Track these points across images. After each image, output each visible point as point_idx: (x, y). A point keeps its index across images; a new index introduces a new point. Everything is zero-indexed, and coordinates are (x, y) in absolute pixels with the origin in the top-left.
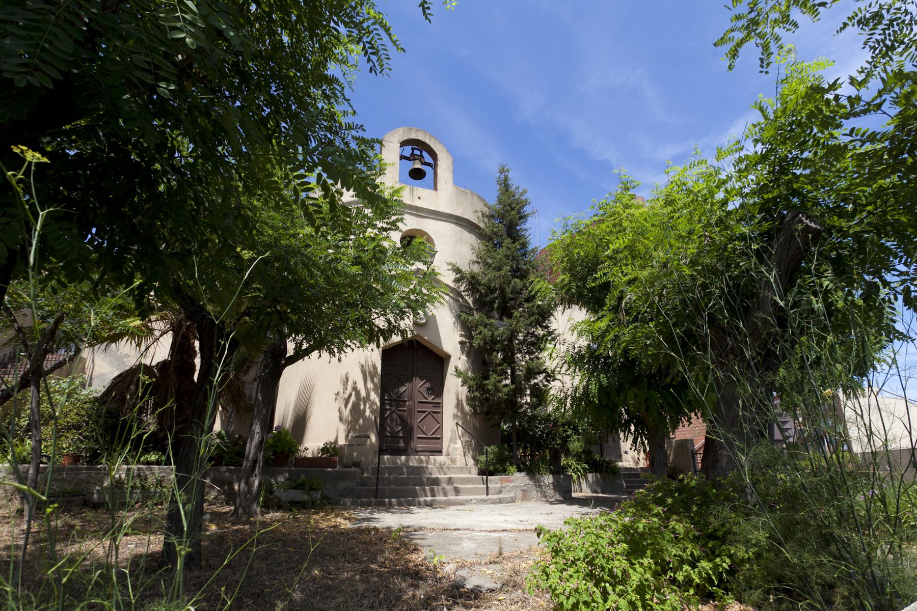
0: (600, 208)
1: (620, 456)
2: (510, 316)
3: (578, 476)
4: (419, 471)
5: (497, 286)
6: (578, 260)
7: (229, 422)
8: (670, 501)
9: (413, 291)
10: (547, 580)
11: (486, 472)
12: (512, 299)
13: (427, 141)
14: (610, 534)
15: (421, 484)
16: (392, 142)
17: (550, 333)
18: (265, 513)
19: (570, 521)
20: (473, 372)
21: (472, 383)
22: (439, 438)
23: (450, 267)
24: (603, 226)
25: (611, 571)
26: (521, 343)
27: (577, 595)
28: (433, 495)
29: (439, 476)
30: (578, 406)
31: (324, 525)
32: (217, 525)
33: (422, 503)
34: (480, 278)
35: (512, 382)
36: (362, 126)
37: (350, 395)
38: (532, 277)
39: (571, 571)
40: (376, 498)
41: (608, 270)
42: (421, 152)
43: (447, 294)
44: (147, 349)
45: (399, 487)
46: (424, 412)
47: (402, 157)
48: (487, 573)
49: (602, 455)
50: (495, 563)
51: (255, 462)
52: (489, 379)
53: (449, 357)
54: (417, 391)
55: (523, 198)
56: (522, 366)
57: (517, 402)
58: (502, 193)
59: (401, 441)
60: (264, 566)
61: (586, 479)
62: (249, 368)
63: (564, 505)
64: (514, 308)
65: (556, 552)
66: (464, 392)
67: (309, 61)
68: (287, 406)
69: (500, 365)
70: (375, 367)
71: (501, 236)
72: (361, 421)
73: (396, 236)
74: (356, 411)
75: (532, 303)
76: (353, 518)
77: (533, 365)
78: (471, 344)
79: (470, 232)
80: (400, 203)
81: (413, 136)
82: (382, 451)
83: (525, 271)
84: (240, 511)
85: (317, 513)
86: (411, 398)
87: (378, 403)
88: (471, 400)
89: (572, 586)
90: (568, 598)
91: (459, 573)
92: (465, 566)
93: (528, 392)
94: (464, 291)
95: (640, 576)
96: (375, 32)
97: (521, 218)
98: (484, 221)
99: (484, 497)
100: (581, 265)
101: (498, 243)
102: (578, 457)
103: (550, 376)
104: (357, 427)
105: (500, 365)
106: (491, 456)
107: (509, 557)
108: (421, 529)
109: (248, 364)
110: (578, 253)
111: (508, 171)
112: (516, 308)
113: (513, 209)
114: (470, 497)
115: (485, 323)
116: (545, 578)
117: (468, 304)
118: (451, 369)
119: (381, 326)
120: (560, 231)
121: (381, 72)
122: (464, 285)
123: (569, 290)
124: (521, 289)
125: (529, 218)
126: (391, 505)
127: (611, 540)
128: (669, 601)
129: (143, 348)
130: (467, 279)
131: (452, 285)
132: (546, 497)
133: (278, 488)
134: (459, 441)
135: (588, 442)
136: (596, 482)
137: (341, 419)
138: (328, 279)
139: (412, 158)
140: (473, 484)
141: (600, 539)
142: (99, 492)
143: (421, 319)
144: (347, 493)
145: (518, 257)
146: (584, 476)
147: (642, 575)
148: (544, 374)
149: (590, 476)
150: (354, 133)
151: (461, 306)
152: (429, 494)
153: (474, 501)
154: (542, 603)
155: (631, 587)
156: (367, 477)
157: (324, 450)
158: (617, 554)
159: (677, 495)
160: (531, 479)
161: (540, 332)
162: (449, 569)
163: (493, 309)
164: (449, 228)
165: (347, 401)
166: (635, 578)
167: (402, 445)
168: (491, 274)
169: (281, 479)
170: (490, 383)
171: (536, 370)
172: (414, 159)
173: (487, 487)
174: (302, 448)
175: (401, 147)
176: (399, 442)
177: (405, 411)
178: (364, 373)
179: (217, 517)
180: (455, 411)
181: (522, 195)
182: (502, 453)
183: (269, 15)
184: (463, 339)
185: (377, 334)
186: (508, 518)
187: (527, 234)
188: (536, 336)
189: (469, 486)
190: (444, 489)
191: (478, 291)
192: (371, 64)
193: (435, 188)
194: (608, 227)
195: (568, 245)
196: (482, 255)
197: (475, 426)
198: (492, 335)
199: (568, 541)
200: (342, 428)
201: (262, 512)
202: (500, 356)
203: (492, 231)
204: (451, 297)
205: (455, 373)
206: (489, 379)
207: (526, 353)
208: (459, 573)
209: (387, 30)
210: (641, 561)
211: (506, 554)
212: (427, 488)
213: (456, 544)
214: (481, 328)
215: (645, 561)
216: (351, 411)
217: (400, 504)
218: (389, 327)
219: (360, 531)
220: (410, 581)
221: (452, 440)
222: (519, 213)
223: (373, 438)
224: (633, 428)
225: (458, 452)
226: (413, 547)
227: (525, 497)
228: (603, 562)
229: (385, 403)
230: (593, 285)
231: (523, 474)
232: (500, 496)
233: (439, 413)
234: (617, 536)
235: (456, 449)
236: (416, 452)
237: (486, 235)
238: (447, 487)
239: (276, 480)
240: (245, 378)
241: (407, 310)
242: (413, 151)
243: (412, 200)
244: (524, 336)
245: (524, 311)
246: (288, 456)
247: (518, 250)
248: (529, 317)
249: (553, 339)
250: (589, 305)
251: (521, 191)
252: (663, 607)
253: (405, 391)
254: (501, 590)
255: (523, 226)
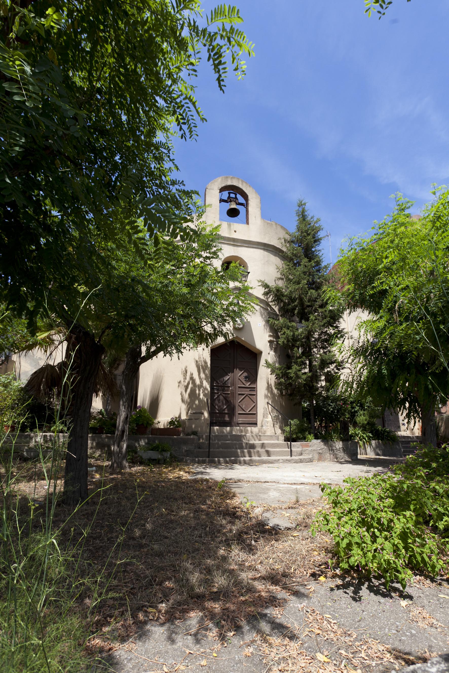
0: (380, 228)
1: (399, 427)
2: (307, 320)
3: (364, 442)
4: (239, 438)
5: (297, 296)
6: (361, 272)
7: (107, 403)
8: (434, 465)
9: (231, 304)
10: (327, 525)
11: (290, 439)
12: (308, 306)
13: (240, 186)
14: (379, 491)
15: (241, 447)
16: (213, 189)
17: (340, 332)
18: (132, 467)
19: (348, 480)
20: (280, 364)
21: (279, 372)
22: (254, 414)
23: (260, 284)
24: (381, 243)
25: (379, 519)
26: (316, 340)
27: (350, 538)
28: (250, 456)
29: (255, 442)
30: (362, 388)
31: (171, 476)
32: (100, 474)
33: (242, 462)
34: (284, 290)
35: (310, 371)
36: (183, 181)
37: (188, 384)
38: (325, 288)
39: (345, 519)
40: (209, 457)
41: (384, 279)
42: (236, 195)
43: (257, 305)
44: (51, 354)
45: (226, 450)
46: (243, 394)
47: (221, 201)
48: (286, 515)
49: (384, 426)
50: (292, 508)
51: (123, 431)
52: (291, 369)
53: (261, 353)
54: (237, 379)
55: (317, 225)
56: (317, 358)
57: (313, 386)
58: (301, 223)
59: (227, 416)
60: (128, 504)
61: (370, 445)
62: (119, 365)
63: (351, 465)
64: (310, 313)
65: (336, 503)
66: (273, 379)
67: (142, 132)
68: (145, 391)
69: (300, 357)
70: (206, 363)
71: (300, 257)
72: (197, 402)
73: (217, 264)
74: (193, 395)
75: (325, 309)
76: (191, 472)
77: (326, 357)
78: (277, 342)
79: (275, 256)
80: (219, 237)
81: (229, 183)
82: (212, 424)
83: (319, 283)
84: (115, 465)
85: (166, 468)
86: (233, 384)
87: (209, 389)
88: (278, 385)
89: (346, 531)
90: (342, 539)
91: (265, 515)
92: (270, 510)
93: (323, 378)
94: (271, 302)
95: (402, 525)
96: (186, 105)
97: (315, 241)
98: (286, 246)
99: (289, 457)
100: (364, 276)
101: (297, 263)
102: (364, 428)
103: (340, 366)
104: (194, 406)
105: (300, 357)
106: (294, 427)
107: (304, 504)
108: (239, 481)
109: (117, 362)
110: (361, 267)
111: (305, 204)
112: (312, 313)
113: (308, 235)
114: (278, 458)
115: (288, 326)
116: (326, 523)
117: (275, 311)
118: (262, 362)
119: (209, 332)
120: (346, 249)
121: (190, 138)
122: (271, 297)
123: (354, 297)
124: (316, 298)
125: (322, 241)
126: (219, 462)
127: (380, 496)
128: (427, 545)
129: (48, 353)
130: (274, 292)
131: (262, 297)
132: (337, 459)
133: (140, 449)
134: (270, 416)
135: (371, 416)
136: (377, 446)
137: (183, 401)
138: (165, 300)
139: (229, 200)
140: (280, 448)
141: (370, 496)
142: (27, 451)
143: (239, 325)
144: (188, 453)
145: (313, 272)
146: (369, 442)
147: (405, 524)
148: (335, 364)
149: (373, 442)
150: (177, 186)
151: (269, 313)
152: (247, 455)
153: (281, 461)
154: (327, 540)
155: (395, 533)
156: (202, 443)
157: (171, 423)
158: (384, 507)
159: (441, 460)
160: (325, 444)
161: (331, 331)
162: (258, 511)
163: (294, 315)
164: (259, 253)
165: (186, 387)
166: (398, 527)
167: (227, 419)
168: (292, 287)
169: (142, 443)
170: (292, 372)
171: (328, 361)
172: (231, 201)
173: (291, 451)
174: (156, 421)
175: (220, 192)
176: (224, 417)
177: (229, 394)
178: (198, 367)
179: (100, 469)
180: (266, 392)
181: (316, 222)
182: (303, 425)
183: (109, 101)
184: (272, 339)
185: (206, 337)
186: (306, 474)
187: (321, 254)
188: (328, 334)
189: (278, 450)
190: (258, 452)
191: (282, 301)
192: (182, 132)
193: (247, 223)
194: (387, 243)
195: (353, 260)
196: (285, 273)
197: (281, 405)
198: (293, 335)
199: (345, 496)
200: (184, 407)
201: (130, 466)
202: (300, 351)
203: (293, 253)
204: (261, 307)
205: (265, 365)
206: (291, 369)
207: (321, 348)
208: (265, 515)
209: (194, 104)
210: (404, 513)
211: (302, 501)
212: (246, 451)
213: (265, 493)
214: (285, 330)
215: (408, 513)
216: (189, 395)
217: (226, 462)
218: (215, 332)
219: (196, 481)
220: (229, 519)
221: (264, 416)
222: (314, 238)
223: (206, 414)
224: (407, 405)
225: (269, 424)
226: (232, 494)
227: (321, 458)
228: (373, 513)
229: (214, 389)
230: (371, 292)
231: (319, 441)
232: (301, 457)
233: (254, 395)
234: (385, 492)
235: (268, 422)
236: (238, 424)
237: (287, 256)
238: (259, 449)
239: (139, 444)
240: (116, 372)
241: (227, 318)
242: (229, 195)
243: (230, 233)
244: (319, 335)
245: (318, 315)
246: (147, 427)
247: (314, 267)
248: (323, 320)
249: (342, 336)
250: (370, 308)
251: (315, 219)
252: (422, 550)
253: (229, 379)
254: (295, 528)
255: (318, 248)
